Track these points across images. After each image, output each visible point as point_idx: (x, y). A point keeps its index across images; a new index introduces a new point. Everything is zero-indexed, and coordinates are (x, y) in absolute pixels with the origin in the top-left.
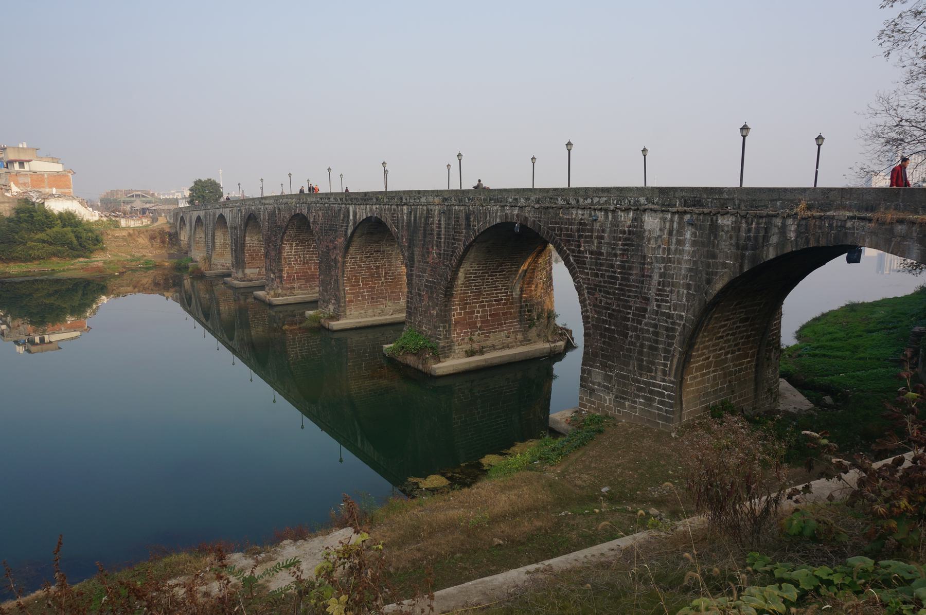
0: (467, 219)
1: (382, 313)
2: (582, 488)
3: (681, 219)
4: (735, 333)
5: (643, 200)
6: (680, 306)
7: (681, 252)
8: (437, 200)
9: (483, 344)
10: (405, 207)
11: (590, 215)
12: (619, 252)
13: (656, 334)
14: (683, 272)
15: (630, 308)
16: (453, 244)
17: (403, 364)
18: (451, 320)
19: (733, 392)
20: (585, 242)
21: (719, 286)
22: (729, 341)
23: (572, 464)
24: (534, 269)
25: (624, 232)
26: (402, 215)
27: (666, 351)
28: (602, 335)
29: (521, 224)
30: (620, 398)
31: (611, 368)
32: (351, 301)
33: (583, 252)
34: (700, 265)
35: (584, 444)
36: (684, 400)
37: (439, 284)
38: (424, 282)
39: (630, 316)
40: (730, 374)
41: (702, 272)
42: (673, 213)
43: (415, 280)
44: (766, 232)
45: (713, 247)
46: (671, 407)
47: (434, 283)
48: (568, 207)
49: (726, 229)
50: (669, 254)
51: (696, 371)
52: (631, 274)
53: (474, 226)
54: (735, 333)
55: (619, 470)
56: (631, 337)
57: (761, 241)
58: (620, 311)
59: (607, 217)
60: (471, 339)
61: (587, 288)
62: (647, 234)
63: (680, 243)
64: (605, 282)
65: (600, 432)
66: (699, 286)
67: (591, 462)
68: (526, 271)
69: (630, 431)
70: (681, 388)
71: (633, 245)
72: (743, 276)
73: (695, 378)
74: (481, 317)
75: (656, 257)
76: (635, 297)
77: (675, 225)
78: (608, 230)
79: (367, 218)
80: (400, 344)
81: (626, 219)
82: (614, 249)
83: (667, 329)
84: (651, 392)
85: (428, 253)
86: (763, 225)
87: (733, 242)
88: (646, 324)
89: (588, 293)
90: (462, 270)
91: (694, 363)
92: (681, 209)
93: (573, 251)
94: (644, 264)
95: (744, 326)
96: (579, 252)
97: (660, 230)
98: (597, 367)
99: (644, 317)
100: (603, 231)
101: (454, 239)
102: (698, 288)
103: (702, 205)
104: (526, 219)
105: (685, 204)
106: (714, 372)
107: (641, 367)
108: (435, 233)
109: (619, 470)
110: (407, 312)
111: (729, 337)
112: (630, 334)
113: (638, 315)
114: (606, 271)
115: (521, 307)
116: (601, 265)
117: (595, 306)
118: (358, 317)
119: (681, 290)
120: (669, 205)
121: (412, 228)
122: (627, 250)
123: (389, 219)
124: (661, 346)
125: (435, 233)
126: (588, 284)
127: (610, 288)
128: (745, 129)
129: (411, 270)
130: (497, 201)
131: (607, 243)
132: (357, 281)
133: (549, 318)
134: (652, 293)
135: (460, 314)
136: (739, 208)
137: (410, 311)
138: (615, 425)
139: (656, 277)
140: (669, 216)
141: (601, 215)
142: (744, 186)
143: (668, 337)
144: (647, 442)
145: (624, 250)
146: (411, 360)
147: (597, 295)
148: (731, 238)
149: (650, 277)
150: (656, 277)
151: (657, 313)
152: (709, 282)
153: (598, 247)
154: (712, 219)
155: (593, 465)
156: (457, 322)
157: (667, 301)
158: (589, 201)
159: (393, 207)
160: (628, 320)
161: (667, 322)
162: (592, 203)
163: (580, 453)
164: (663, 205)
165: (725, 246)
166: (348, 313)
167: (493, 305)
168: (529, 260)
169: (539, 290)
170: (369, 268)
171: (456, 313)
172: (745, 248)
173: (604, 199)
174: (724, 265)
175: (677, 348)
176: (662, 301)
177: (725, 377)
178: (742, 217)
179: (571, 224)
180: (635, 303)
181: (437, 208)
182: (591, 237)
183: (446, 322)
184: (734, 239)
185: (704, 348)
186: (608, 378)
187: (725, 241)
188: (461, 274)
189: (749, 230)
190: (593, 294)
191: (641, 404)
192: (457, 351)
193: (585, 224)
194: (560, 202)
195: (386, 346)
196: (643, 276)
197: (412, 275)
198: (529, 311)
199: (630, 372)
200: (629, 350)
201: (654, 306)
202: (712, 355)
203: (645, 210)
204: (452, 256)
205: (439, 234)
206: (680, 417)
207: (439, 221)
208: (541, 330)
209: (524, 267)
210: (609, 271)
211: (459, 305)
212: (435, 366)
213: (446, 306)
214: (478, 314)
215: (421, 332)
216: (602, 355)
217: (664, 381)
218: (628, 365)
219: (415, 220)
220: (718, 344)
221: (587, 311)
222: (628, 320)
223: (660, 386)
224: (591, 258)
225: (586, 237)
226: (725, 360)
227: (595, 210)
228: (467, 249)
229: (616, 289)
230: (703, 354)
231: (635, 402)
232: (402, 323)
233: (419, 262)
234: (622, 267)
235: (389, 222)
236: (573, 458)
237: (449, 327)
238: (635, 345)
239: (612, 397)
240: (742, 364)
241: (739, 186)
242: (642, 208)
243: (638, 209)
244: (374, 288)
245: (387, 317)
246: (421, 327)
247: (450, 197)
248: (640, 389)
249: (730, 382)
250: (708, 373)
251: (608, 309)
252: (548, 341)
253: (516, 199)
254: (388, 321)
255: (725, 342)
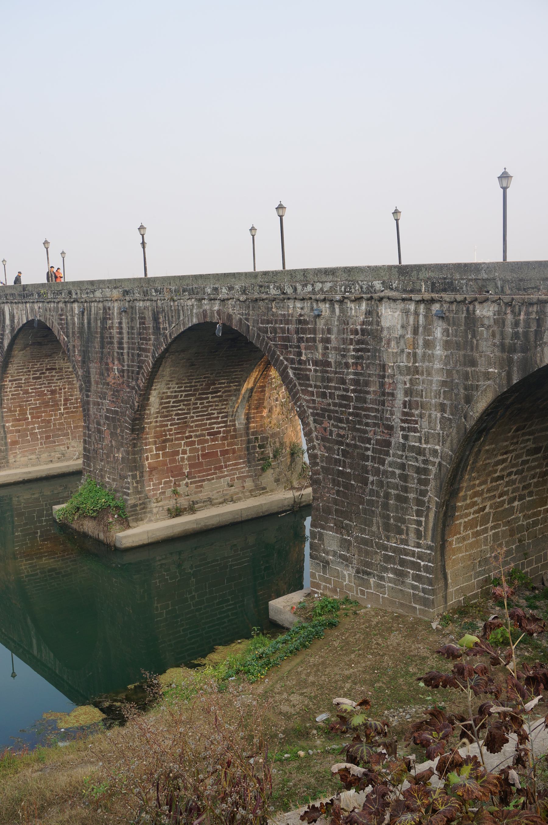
0: (156, 319)
1: (63, 457)
2: (288, 717)
3: (428, 310)
4: (523, 471)
5: (378, 285)
6: (434, 437)
7: (430, 358)
8: (116, 294)
9: (194, 498)
10: (76, 305)
11: (312, 309)
12: (351, 361)
13: (404, 478)
14: (435, 387)
15: (369, 441)
16: (139, 355)
17: (78, 533)
18: (143, 466)
19: (526, 555)
20: (306, 349)
21: (482, 404)
22: (513, 482)
23: (282, 679)
24: (263, 387)
25: (356, 332)
26: (73, 316)
27: (420, 503)
28: (335, 483)
29: (224, 324)
30: (362, 573)
31: (348, 529)
32: (15, 443)
33: (305, 363)
34: (455, 376)
35: (305, 646)
36: (449, 572)
37: (123, 414)
38: (103, 412)
39: (369, 453)
40: (520, 529)
41: (460, 389)
42: (418, 302)
43: (93, 410)
44: (539, 325)
45: (472, 350)
46: (430, 584)
47: (116, 412)
48: (284, 298)
49: (486, 322)
50: (415, 362)
51: (465, 528)
52: (368, 393)
53: (165, 329)
54: (523, 471)
55: (348, 685)
56: (372, 483)
57: (532, 339)
58: (355, 446)
59: (333, 311)
60: (175, 492)
61: (313, 414)
62: (385, 333)
63: (428, 344)
64: (335, 405)
65: (332, 625)
66: (456, 407)
67: (308, 675)
68: (252, 390)
69: (375, 621)
70: (443, 554)
71: (368, 350)
72: (513, 389)
73: (464, 539)
74: (189, 458)
75: (399, 367)
76: (375, 425)
77: (421, 319)
78: (335, 330)
79: (28, 322)
80: (75, 503)
81: (358, 312)
82: (344, 356)
83: (418, 470)
84: (403, 563)
85: (108, 370)
86: (534, 316)
87: (497, 341)
88: (390, 465)
89: (315, 421)
90: (154, 393)
91: (461, 517)
92: (427, 296)
93: (292, 361)
94: (384, 377)
95: (534, 460)
96: (300, 362)
97: (403, 327)
98: (331, 529)
99: (387, 454)
100: (329, 331)
101: (140, 349)
102: (455, 410)
103: (454, 290)
104: (230, 317)
105: (433, 288)
106: (493, 528)
107: (387, 527)
108: (115, 340)
109: (348, 685)
110: (85, 457)
111: (513, 477)
112: (371, 478)
113: (380, 452)
114: (336, 388)
115: (249, 441)
116: (329, 380)
117: (324, 439)
118: (26, 466)
119: (434, 413)
120: (412, 291)
121: (86, 335)
122: (361, 357)
123: (56, 324)
124: (412, 496)
125: (115, 340)
126: (314, 408)
127: (342, 413)
128: (505, 177)
129: (88, 396)
130: (192, 292)
131: (336, 349)
132: (23, 412)
133: (292, 454)
134: (396, 420)
135: (157, 456)
136: (502, 291)
137: (88, 456)
138: (355, 613)
139: (400, 396)
140: (412, 307)
141: (325, 307)
142: (509, 260)
143: (421, 482)
144: (395, 639)
145: (357, 358)
146: (89, 527)
147: (326, 424)
148: (494, 335)
149: (393, 395)
150: (400, 396)
151: (403, 447)
152: (468, 400)
153: (324, 355)
154: (468, 310)
155: (311, 679)
156: (153, 469)
157: (415, 430)
158: (309, 288)
159: (61, 305)
160: (366, 458)
161: (417, 460)
162: (313, 292)
163: (298, 660)
164: (405, 291)
165: (487, 348)
166: (11, 459)
167: (206, 441)
168: (255, 374)
169: (274, 416)
170: (41, 394)
171: (151, 455)
172: (512, 349)
173: (329, 285)
174: (487, 376)
175: (432, 497)
176: (410, 429)
177: (511, 535)
178: (507, 304)
179: (288, 322)
180: (375, 434)
181: (116, 304)
182: (314, 340)
183: (135, 468)
184: (498, 336)
185: (476, 494)
186: (345, 544)
187: (487, 340)
188: (154, 399)
189: (516, 324)
190: (321, 423)
191: (390, 580)
192: (155, 510)
193: (306, 322)
194: (273, 291)
195: (57, 507)
196: (384, 394)
197: (88, 403)
198: (260, 447)
199: (373, 534)
200: (371, 503)
201: (398, 438)
202: (488, 504)
203: (381, 299)
204: (138, 373)
205: (120, 343)
206: (445, 598)
207: (120, 323)
208: (280, 473)
209: (248, 385)
210: (339, 389)
211: (155, 443)
212: (121, 534)
213: (135, 446)
214: (185, 456)
215: (103, 486)
216: (336, 510)
217: (418, 546)
218: (370, 525)
219: (89, 323)
220: (496, 488)
221: (314, 447)
222: (366, 458)
223: (413, 554)
224: (316, 371)
225: (308, 340)
226: (511, 511)
227: (317, 301)
228: (158, 363)
229: (350, 414)
230: (474, 504)
231: (382, 578)
232: (77, 474)
233: (97, 383)
234: (356, 382)
235: (56, 328)
236: (286, 668)
237: (142, 476)
238: (378, 496)
239: (352, 571)
240: (538, 514)
241: (501, 260)
242: (376, 296)
243: (371, 298)
244: (49, 421)
245: (71, 463)
246: (102, 477)
247: (133, 289)
248: (387, 559)
249: (520, 541)
250: (485, 531)
251: (341, 443)
252: (292, 488)
253: (216, 289)
254: (71, 469)
255: (508, 484)
